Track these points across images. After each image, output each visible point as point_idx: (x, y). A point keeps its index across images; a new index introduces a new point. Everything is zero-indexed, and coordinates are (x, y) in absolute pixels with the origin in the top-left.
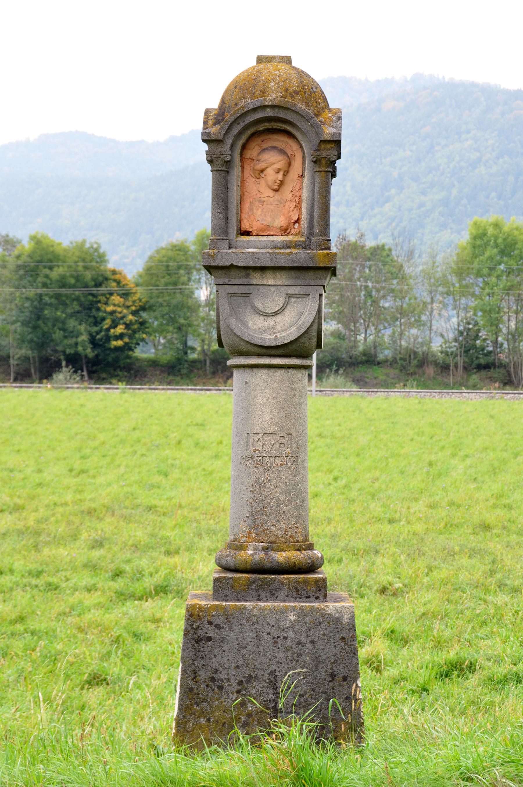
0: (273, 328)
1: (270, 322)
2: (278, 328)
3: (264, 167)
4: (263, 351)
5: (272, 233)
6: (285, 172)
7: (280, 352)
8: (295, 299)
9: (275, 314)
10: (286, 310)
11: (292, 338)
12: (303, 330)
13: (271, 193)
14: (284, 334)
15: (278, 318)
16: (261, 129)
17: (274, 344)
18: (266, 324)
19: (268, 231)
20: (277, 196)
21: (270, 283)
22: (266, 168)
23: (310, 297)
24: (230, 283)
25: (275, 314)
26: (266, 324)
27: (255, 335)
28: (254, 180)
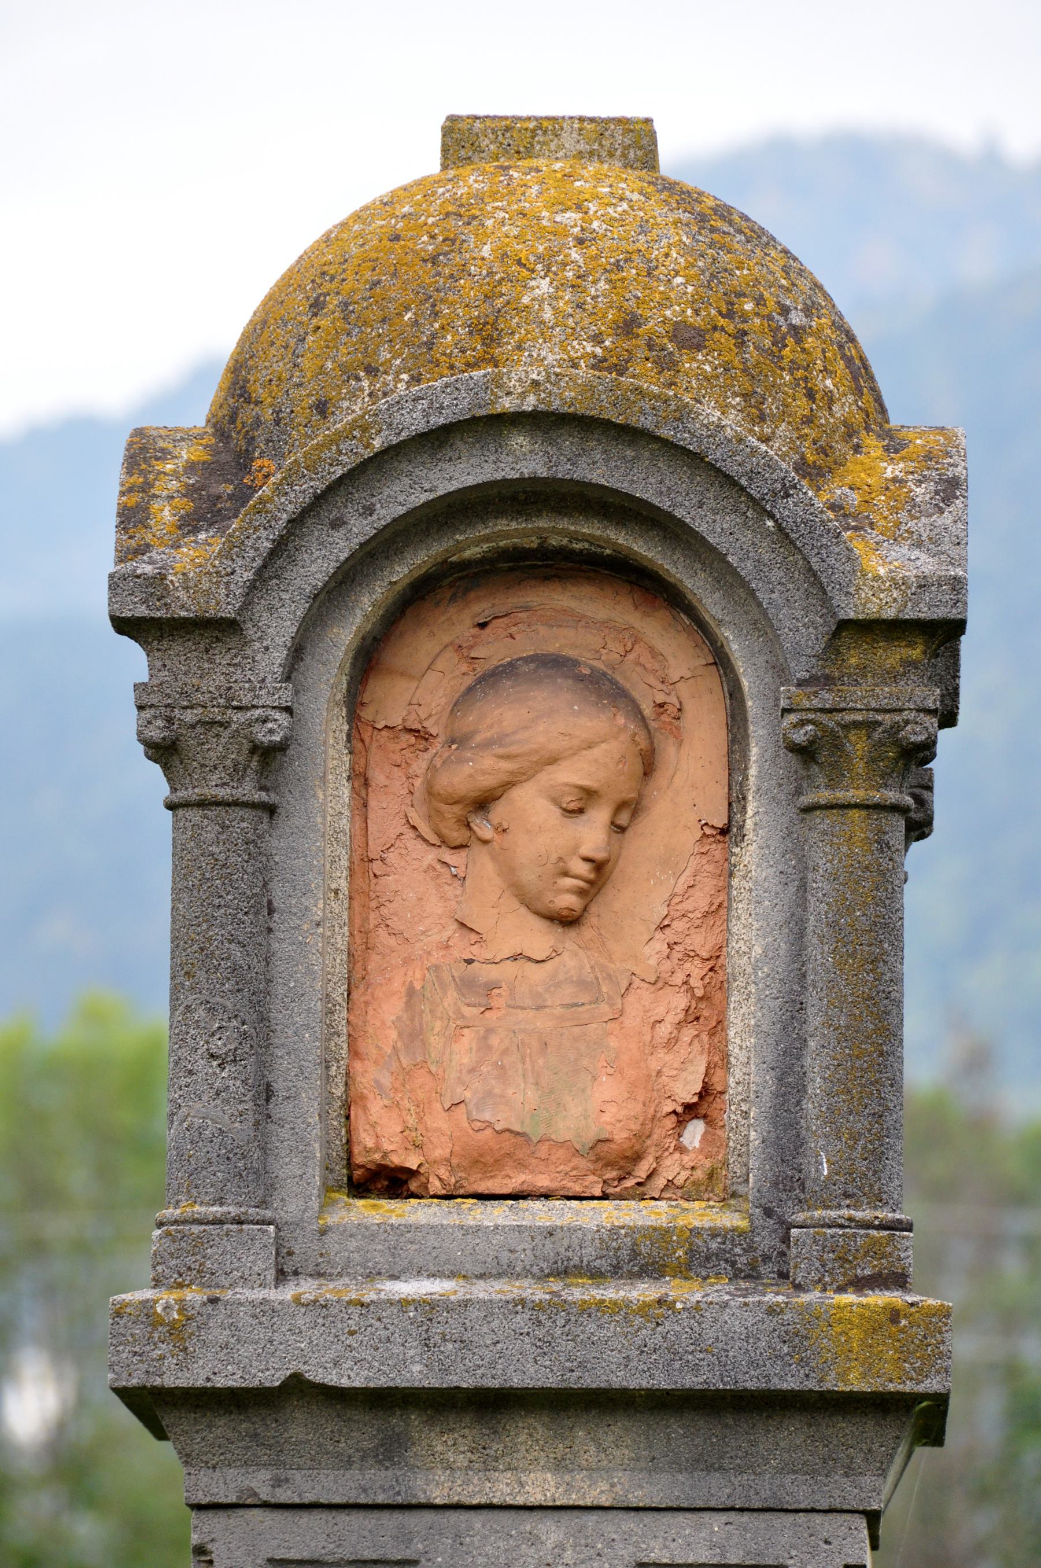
5: (543, 1182)
19: (521, 1165)
21: (536, 1497)
22: (508, 785)
28: (430, 856)
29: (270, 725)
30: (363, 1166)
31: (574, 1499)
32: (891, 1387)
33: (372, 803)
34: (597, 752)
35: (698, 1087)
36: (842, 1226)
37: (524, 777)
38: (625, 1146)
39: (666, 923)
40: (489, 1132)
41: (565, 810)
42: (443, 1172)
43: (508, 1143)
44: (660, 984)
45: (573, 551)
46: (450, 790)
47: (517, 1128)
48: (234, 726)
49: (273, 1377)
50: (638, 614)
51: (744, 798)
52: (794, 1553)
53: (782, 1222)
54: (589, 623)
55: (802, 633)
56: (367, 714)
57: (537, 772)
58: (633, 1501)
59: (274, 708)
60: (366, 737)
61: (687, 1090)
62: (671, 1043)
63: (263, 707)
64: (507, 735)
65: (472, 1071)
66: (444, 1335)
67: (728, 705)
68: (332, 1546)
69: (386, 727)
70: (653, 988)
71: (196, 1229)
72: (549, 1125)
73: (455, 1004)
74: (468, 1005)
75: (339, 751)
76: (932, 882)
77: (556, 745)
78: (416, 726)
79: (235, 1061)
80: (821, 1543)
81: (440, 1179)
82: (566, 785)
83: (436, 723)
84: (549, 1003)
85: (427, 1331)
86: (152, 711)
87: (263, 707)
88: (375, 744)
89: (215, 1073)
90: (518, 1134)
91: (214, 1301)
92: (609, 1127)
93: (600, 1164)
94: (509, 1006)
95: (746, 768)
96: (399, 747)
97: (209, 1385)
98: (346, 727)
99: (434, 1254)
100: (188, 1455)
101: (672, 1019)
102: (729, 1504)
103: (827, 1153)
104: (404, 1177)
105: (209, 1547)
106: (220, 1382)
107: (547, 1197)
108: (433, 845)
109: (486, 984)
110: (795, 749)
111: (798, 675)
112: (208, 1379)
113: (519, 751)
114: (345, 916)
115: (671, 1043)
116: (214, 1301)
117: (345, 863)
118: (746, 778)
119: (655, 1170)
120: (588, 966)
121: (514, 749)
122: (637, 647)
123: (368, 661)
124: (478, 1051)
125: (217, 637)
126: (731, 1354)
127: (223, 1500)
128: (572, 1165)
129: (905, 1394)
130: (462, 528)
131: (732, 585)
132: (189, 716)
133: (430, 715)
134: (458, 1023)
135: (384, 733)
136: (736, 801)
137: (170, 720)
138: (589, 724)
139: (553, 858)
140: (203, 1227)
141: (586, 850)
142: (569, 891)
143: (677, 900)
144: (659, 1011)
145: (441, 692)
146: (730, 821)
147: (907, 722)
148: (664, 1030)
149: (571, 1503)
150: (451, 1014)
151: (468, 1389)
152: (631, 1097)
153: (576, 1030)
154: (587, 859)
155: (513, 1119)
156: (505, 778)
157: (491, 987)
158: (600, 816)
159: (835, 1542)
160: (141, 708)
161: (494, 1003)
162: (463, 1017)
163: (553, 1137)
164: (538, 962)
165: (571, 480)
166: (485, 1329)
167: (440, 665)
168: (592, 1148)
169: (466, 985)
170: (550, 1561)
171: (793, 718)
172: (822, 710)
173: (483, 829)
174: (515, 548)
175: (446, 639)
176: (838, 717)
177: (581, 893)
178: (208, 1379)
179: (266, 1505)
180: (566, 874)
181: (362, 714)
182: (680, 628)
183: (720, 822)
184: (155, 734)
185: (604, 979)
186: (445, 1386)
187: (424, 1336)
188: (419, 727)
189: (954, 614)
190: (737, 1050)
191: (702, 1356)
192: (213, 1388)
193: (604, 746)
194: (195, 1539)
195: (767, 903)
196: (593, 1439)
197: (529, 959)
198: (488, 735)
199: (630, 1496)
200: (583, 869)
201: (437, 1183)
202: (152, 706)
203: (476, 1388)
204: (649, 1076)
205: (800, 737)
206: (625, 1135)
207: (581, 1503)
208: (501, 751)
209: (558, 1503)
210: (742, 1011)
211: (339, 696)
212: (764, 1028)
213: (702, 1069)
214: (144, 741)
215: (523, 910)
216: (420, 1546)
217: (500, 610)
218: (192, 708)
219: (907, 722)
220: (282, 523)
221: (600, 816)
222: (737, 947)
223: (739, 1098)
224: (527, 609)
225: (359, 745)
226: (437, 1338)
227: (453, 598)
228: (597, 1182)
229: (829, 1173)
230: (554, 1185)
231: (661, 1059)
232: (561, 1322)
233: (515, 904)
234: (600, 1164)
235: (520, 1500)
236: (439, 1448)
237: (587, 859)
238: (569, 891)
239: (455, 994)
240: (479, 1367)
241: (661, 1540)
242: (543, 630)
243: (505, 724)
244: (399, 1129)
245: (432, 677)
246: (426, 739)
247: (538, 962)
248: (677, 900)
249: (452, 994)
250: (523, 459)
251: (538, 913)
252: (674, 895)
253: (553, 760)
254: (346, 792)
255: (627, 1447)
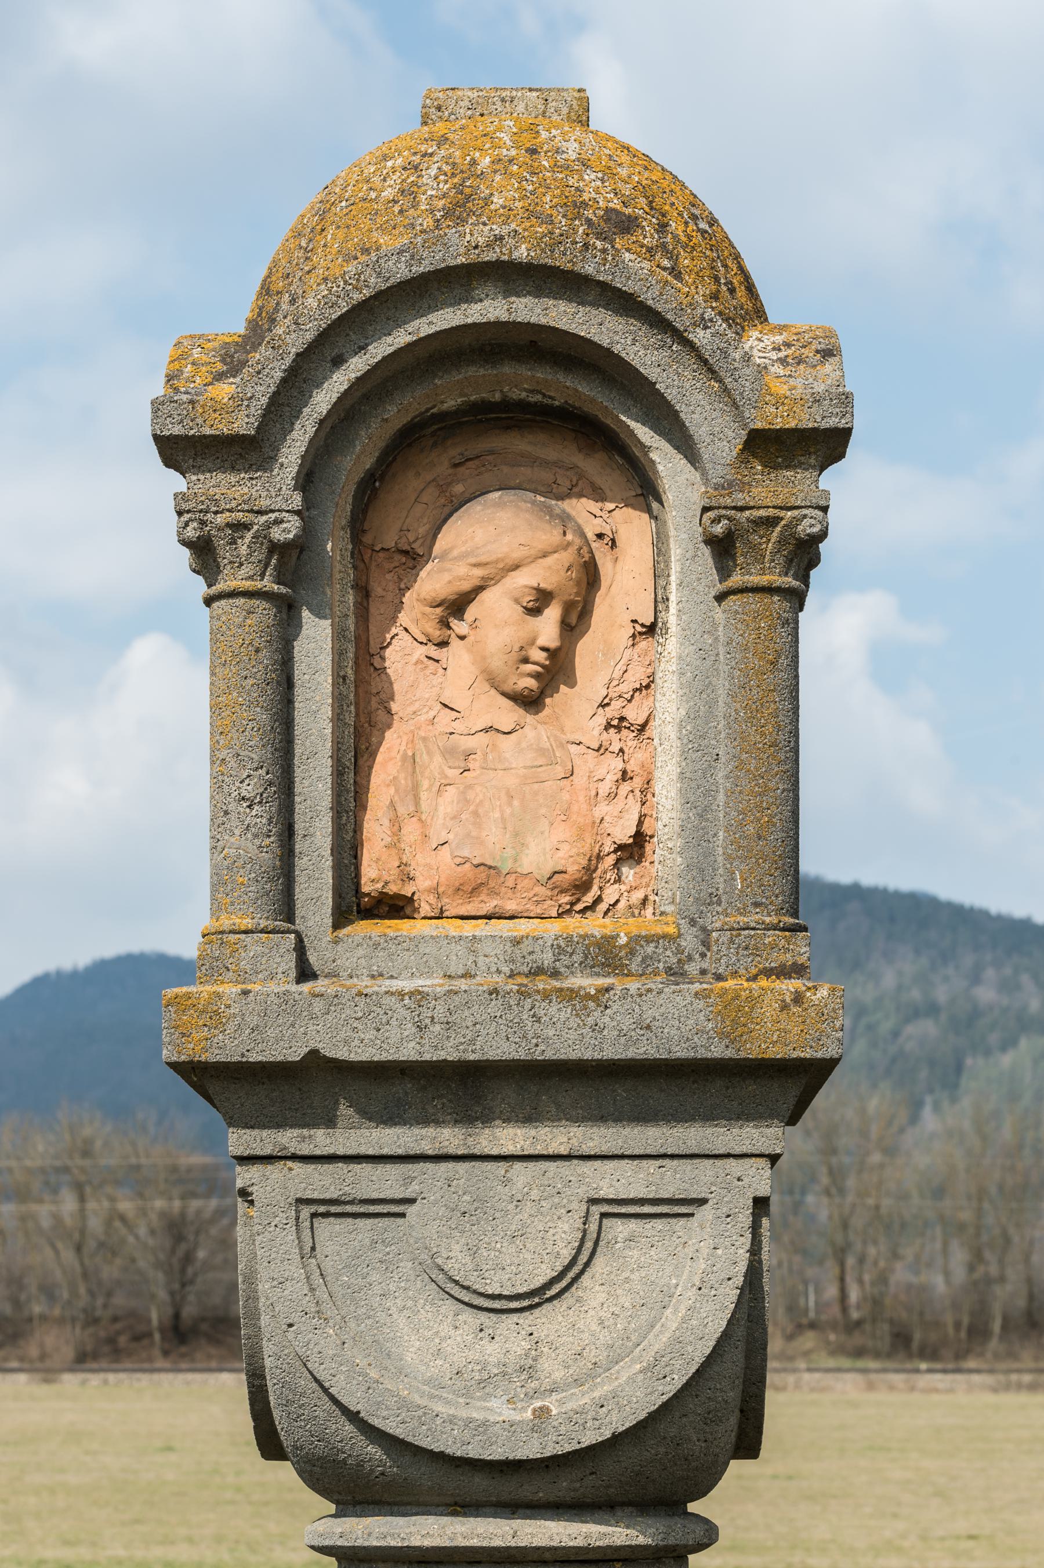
0: (528, 1370)
1: (510, 1338)
2: (552, 1369)
3: (466, 586)
4: (480, 1484)
5: (511, 906)
6: (568, 607)
7: (564, 1486)
8: (633, 1225)
9: (536, 1298)
10: (585, 1280)
11: (619, 1421)
12: (678, 1381)
13: (508, 714)
14: (581, 1399)
15: (547, 1321)
16: (451, 403)
17: (531, 1449)
18: (492, 1351)
19: (494, 893)
20: (535, 729)
21: (510, 1149)
22: (478, 589)
23: (705, 1213)
24: (306, 1150)
25: (536, 1298)
26: (492, 1351)
27: (439, 1408)
28: (421, 651)
29: (285, 525)
30: (368, 895)
31: (539, 1149)
32: (795, 1055)
33: (373, 610)
34: (550, 560)
35: (632, 831)
36: (754, 929)
37: (493, 582)
38: (576, 877)
39: (606, 701)
40: (467, 865)
41: (525, 608)
42: (432, 899)
43: (482, 875)
44: (602, 751)
45: (529, 404)
46: (434, 595)
47: (489, 863)
48: (256, 527)
49: (295, 1053)
50: (581, 456)
51: (668, 600)
52: (713, 1189)
53: (704, 929)
54: (545, 464)
55: (719, 436)
56: (367, 539)
57: (503, 577)
58: (586, 1150)
59: (288, 511)
60: (366, 557)
61: (624, 833)
62: (612, 796)
63: (279, 511)
64: (478, 548)
65: (454, 818)
66: (433, 1018)
67: (654, 530)
68: (346, 1188)
69: (383, 549)
70: (597, 753)
71: (232, 938)
72: (515, 860)
73: (440, 767)
74: (450, 767)
75: (345, 566)
76: (836, 627)
77: (517, 555)
78: (406, 547)
79: (260, 803)
80: (735, 1180)
81: (430, 904)
82: (526, 586)
83: (422, 545)
84: (513, 766)
85: (419, 1016)
86: (189, 515)
87: (279, 511)
88: (374, 564)
89: (245, 812)
90: (490, 867)
91: (246, 993)
92: (563, 861)
93: (556, 891)
94: (483, 768)
95: (669, 576)
96: (393, 565)
97: (244, 1060)
98: (350, 547)
99: (424, 959)
100: (231, 1118)
101: (611, 778)
102: (662, 1151)
103: (741, 872)
104: (401, 904)
105: (250, 1190)
106: (254, 1057)
107: (512, 917)
108: (421, 643)
109: (464, 751)
110: (711, 541)
111: (714, 481)
112: (243, 1055)
113: (488, 560)
114: (352, 696)
115: (612, 796)
116: (246, 993)
117: (351, 655)
118: (668, 583)
119: (600, 897)
120: (545, 737)
121: (483, 559)
122: (580, 482)
123: (370, 490)
124: (458, 803)
125: (240, 454)
126: (666, 1031)
127: (452, 1151)
128: (533, 892)
129: (805, 1059)
130: (440, 374)
131: (658, 418)
132: (220, 519)
133: (418, 539)
134: (443, 781)
135: (381, 554)
136: (660, 602)
137: (203, 523)
138: (544, 537)
139: (516, 648)
140: (238, 936)
141: (542, 641)
142: (530, 675)
143: (615, 683)
144: (600, 773)
145: (425, 520)
146: (656, 618)
147: (805, 516)
148: (605, 788)
149: (537, 1152)
150: (436, 774)
151: (452, 1061)
152: (580, 838)
153: (536, 786)
154: (543, 649)
155: (487, 856)
156: (477, 582)
157: (468, 755)
158: (553, 614)
159: (746, 1180)
160: (180, 513)
161: (471, 766)
162: (446, 777)
163: (519, 870)
164: (505, 733)
165: (529, 323)
166: (466, 1013)
167: (425, 498)
168: (549, 878)
169: (449, 752)
170: (520, 1198)
171: (711, 514)
172: (735, 508)
173: (459, 627)
174: (483, 401)
175: (429, 477)
176: (747, 513)
177: (537, 676)
178: (243, 1055)
179: (294, 1157)
180: (526, 660)
181: (364, 540)
182: (615, 466)
183: (648, 620)
184: (191, 533)
185: (557, 747)
186: (434, 1059)
187: (417, 1019)
188: (409, 548)
189: (842, 424)
190: (663, 800)
191: (642, 1032)
192: (247, 1062)
193: (556, 555)
194: (239, 1184)
195: (689, 674)
196: (553, 1102)
197: (498, 731)
198: (463, 549)
199: (584, 1146)
200: (540, 656)
201: (428, 908)
202: (188, 511)
203: (459, 1061)
204: (594, 823)
205: (719, 529)
206: (576, 868)
207: (545, 1153)
208: (473, 560)
209: (526, 1153)
210: (667, 769)
211: (344, 522)
212: (688, 775)
213: (636, 817)
214: (185, 543)
215: (493, 692)
216: (417, 1187)
217: (469, 454)
218: (221, 512)
219: (805, 516)
220: (292, 356)
221: (553, 614)
222: (663, 718)
223: (666, 837)
224: (492, 452)
225: (361, 566)
226: (428, 1021)
227: (435, 445)
228: (554, 906)
229: (742, 887)
230: (520, 908)
231: (602, 809)
232: (528, 1006)
233: (487, 687)
234: (556, 891)
235: (495, 1152)
236: (431, 1111)
237: (543, 649)
238: (530, 675)
239: (440, 759)
240: (462, 1044)
241: (607, 1180)
242: (506, 469)
243: (476, 539)
244: (397, 864)
245: (419, 508)
246: (414, 559)
247: (505, 733)
248: (615, 683)
249: (438, 759)
250: (490, 308)
251: (504, 694)
252: (611, 680)
253: (516, 567)
254: (351, 598)
255: (581, 1108)
